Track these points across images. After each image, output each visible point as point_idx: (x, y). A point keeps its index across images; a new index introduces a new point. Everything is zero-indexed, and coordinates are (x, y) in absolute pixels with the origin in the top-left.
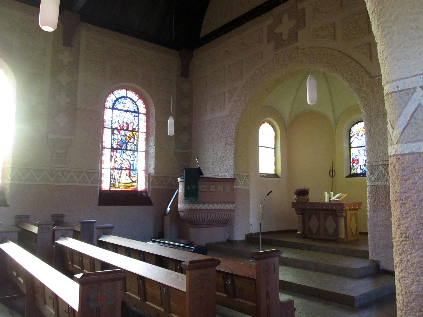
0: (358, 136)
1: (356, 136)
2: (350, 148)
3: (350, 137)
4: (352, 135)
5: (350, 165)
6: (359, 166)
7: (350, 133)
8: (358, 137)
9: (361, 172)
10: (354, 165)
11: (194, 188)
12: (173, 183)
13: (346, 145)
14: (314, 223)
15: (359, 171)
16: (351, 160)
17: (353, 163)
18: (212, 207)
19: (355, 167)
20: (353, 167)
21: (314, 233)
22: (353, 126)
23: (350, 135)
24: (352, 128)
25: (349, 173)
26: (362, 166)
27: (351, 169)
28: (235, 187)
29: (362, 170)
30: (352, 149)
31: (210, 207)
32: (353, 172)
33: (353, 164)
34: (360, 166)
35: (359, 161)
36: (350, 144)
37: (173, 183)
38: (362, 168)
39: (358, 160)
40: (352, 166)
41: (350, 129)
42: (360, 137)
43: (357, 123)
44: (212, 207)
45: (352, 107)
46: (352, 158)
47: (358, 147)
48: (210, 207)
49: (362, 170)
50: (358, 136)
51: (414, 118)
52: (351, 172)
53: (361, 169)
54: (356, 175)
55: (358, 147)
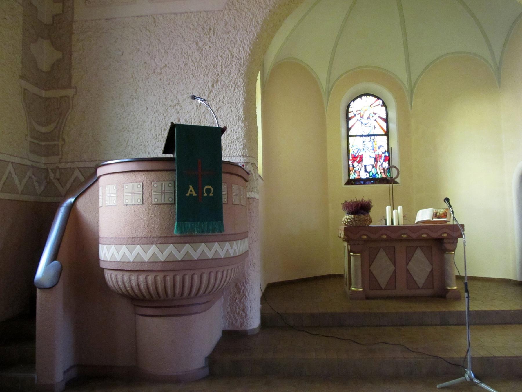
0: (362, 117)
1: (358, 117)
2: (348, 136)
3: (348, 119)
4: (350, 115)
5: (349, 165)
6: (363, 167)
7: (347, 112)
8: (362, 120)
9: (368, 176)
10: (356, 164)
11: (208, 191)
12: (17, 182)
13: (343, 131)
14: (383, 267)
15: (364, 176)
16: (351, 158)
17: (354, 161)
18: (207, 251)
19: (356, 168)
20: (354, 167)
21: (383, 286)
22: (354, 100)
23: (347, 115)
24: (351, 104)
25: (347, 178)
26: (367, 167)
27: (349, 171)
28: (249, 195)
29: (369, 173)
30: (350, 138)
31: (199, 251)
32: (352, 177)
33: (353, 163)
34: (365, 166)
35: (363, 159)
36: (348, 130)
37: (17, 182)
38: (368, 170)
39: (361, 157)
40: (351, 167)
41: (349, 106)
42: (365, 120)
43: (360, 96)
44: (207, 251)
45: (358, 68)
46: (351, 152)
47: (362, 136)
48: (199, 251)
49: (369, 173)
50: (362, 117)
51: (200, 122)
52: (349, 176)
53: (366, 171)
54: (358, 181)
55: (362, 136)
